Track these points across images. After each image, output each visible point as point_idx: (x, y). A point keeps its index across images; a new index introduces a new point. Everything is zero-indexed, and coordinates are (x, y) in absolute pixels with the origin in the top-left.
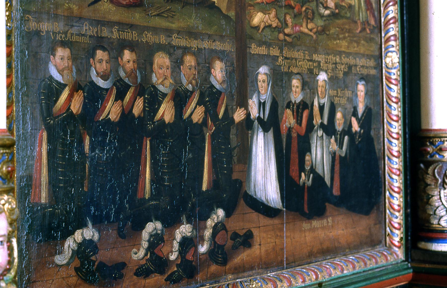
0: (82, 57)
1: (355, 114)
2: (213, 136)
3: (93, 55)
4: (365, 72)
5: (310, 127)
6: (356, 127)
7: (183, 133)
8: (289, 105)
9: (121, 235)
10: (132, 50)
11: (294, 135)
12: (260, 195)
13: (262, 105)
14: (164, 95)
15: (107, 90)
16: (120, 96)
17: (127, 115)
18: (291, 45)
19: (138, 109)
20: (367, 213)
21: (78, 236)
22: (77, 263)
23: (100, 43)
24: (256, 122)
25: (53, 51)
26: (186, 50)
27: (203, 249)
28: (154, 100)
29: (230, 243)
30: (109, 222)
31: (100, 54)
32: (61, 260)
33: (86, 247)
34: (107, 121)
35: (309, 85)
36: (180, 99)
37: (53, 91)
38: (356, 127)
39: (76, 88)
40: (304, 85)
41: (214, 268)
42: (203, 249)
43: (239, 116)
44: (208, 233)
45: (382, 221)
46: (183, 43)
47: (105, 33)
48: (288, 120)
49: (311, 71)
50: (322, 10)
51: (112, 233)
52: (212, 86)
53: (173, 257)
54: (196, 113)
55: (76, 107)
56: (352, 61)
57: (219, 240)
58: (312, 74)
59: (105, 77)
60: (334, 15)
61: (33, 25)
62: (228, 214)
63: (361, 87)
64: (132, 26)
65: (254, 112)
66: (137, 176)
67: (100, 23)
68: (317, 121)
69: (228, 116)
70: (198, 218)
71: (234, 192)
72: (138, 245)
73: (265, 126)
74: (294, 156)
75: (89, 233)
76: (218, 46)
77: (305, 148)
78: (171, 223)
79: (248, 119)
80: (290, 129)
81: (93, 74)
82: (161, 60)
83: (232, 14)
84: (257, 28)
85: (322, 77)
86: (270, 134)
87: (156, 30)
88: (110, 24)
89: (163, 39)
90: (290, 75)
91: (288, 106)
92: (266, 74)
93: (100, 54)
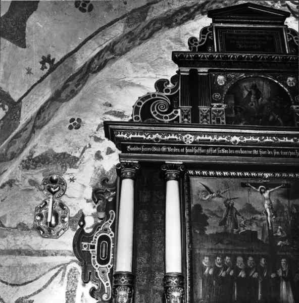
3: (216, 258)
10: (228, 256)
13: (284, 272)
14: (241, 269)
15: (220, 268)
17: (228, 275)
19: (231, 273)
23: (218, 255)
24: (281, 278)
26: (249, 256)
28: (237, 271)
31: (218, 258)
34: (221, 277)
36: (247, 270)
43: (273, 276)
52: (261, 266)
55: (211, 272)
59: (219, 264)
65: (280, 274)
73: (286, 279)
79: (277, 278)
81: (204, 199)
82: (240, 259)
87: (237, 250)
88: (221, 250)
89: (240, 253)
92: (284, 261)
93: (218, 258)
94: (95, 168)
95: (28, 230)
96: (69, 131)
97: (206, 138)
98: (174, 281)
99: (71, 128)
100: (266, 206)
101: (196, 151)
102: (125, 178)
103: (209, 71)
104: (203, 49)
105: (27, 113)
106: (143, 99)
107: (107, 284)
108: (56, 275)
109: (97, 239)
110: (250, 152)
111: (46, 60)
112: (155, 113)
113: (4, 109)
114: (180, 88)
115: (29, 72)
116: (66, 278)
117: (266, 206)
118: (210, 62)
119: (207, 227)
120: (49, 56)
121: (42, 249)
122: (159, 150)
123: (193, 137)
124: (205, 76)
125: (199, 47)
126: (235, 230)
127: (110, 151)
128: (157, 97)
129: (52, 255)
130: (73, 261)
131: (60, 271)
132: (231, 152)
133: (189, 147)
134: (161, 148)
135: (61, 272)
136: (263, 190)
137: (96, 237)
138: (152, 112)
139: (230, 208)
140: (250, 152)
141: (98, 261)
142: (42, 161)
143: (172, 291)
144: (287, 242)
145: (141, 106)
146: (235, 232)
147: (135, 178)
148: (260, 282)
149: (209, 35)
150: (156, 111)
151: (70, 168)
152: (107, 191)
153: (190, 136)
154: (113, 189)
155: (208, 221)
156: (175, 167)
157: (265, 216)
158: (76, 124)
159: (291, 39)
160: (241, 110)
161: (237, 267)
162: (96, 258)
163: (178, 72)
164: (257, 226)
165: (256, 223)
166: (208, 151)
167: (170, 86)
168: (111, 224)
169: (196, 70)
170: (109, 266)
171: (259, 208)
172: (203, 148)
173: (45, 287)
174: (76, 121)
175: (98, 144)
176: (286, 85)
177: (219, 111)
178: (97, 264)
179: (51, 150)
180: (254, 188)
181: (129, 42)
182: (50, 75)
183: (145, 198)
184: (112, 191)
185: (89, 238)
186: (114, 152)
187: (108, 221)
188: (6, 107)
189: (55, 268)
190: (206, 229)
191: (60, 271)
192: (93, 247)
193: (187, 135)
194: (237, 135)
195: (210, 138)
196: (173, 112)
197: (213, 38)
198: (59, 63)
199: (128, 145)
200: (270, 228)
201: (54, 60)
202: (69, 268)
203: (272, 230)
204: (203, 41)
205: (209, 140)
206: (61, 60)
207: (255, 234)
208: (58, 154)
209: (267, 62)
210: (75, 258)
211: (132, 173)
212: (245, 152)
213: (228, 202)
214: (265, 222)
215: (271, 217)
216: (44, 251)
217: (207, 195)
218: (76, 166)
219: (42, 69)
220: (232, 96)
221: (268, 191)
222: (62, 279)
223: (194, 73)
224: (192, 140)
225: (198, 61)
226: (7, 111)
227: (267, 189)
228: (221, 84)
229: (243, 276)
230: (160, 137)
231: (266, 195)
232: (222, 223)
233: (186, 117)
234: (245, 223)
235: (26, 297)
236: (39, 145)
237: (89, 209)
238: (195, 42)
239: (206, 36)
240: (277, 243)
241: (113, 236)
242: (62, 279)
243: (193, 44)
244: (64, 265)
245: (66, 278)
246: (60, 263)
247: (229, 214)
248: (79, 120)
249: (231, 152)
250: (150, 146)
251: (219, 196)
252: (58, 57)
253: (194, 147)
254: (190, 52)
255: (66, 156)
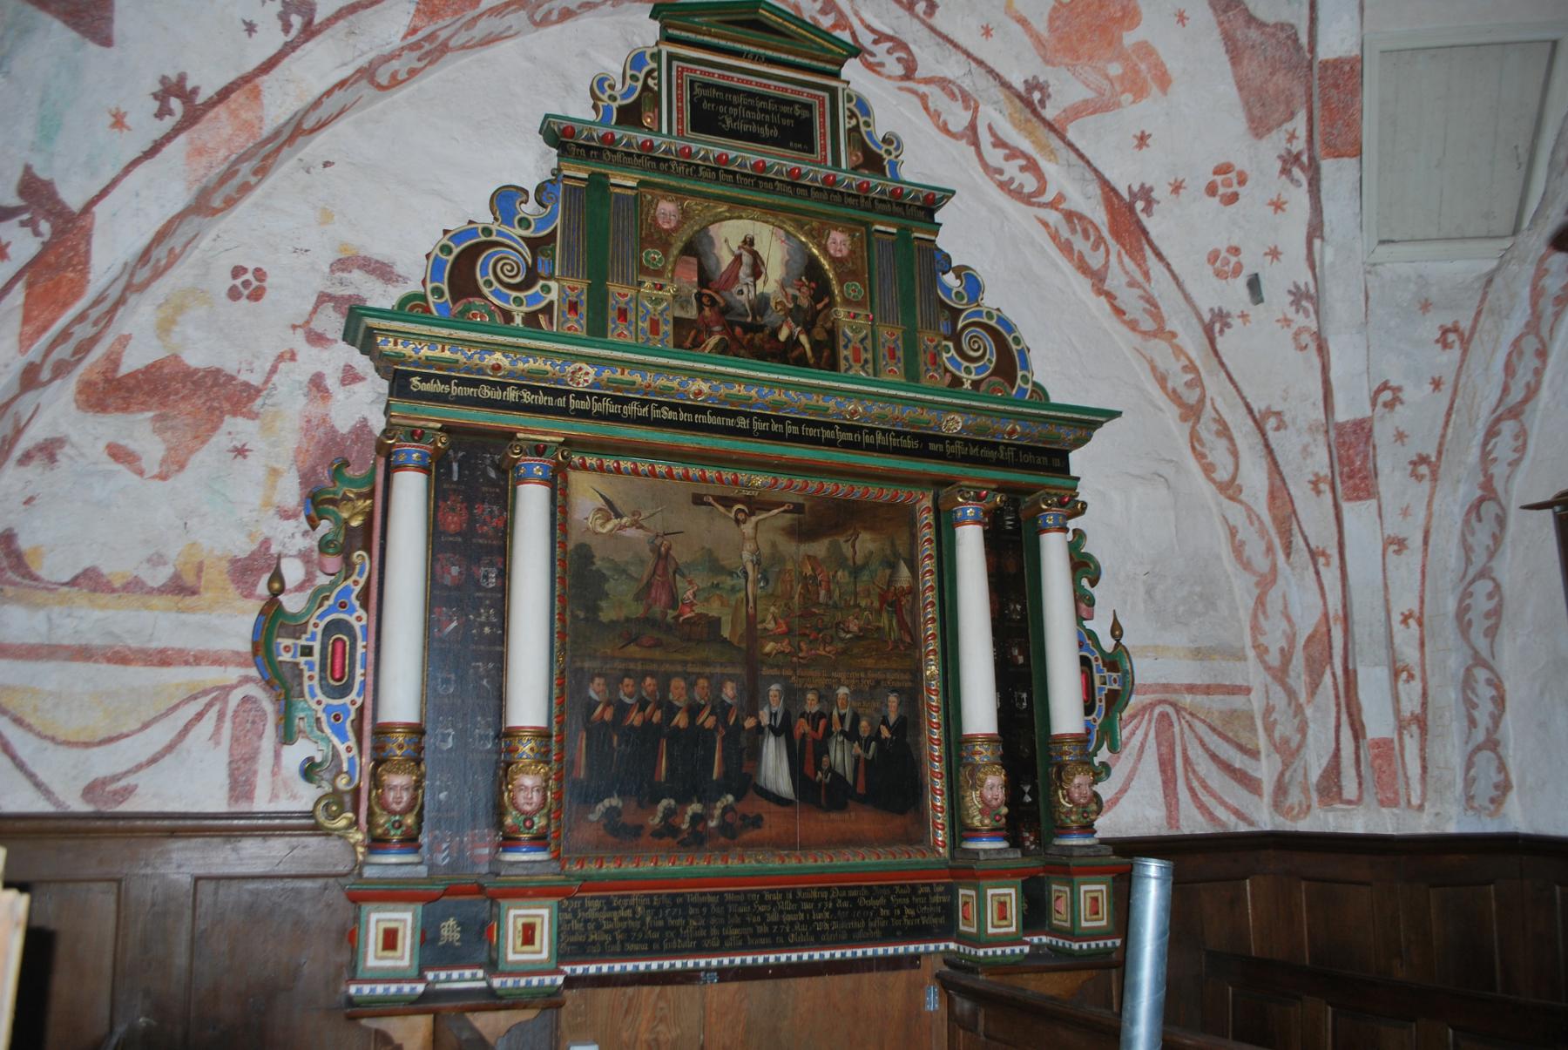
0: (614, 683)
1: (885, 721)
2: (723, 739)
4: (898, 685)
5: (828, 733)
6: (885, 733)
7: (696, 739)
8: (803, 715)
9: (640, 804)
11: (809, 739)
12: (771, 786)
13: (773, 715)
16: (642, 708)
17: (647, 722)
18: (806, 666)
19: (657, 717)
20: (902, 812)
21: (607, 802)
22: (605, 821)
23: (627, 673)
25: (592, 680)
27: (713, 824)
28: (671, 710)
29: (739, 823)
30: (531, 17)
31: (626, 680)
32: (593, 817)
33: (611, 811)
34: (632, 727)
35: (827, 696)
36: (694, 710)
37: (592, 705)
38: (885, 733)
39: (608, 704)
40: (820, 698)
41: (722, 840)
42: (713, 824)
43: (749, 723)
44: (717, 812)
45: (922, 819)
46: (697, 670)
47: (632, 666)
48: (802, 726)
49: (829, 687)
50: (843, 635)
51: (633, 804)
53: (685, 826)
54: (707, 720)
55: (608, 716)
56: (879, 675)
57: (728, 818)
58: (831, 689)
59: (630, 696)
60: (857, 638)
61: (578, 664)
62: (737, 799)
63: (893, 699)
64: (652, 661)
65: (765, 720)
66: (654, 767)
67: (626, 660)
68: (837, 727)
69: (739, 726)
70: (708, 799)
71: (744, 781)
72: (654, 814)
73: (776, 732)
74: (809, 757)
75: (615, 801)
76: (729, 670)
77: (822, 749)
78: (684, 800)
79: (759, 729)
80: (804, 735)
81: (600, 530)
82: (678, 684)
83: (743, 646)
84: (768, 655)
85: (843, 691)
86: (782, 739)
87: (672, 662)
88: (635, 660)
89: (679, 668)
90: (804, 691)
91: (803, 715)
93: (626, 680)
94: (309, 421)
95: (113, 591)
96: (229, 302)
97: (627, 377)
98: (526, 748)
99: (234, 294)
100: (746, 555)
101: (597, 407)
102: (402, 467)
103: (642, 183)
104: (630, 115)
105: (112, 247)
106: (458, 237)
107: (349, 749)
108: (200, 716)
109: (319, 631)
110: (730, 422)
111: (173, 89)
112: (489, 283)
113: (37, 233)
114: (558, 221)
115: (119, 121)
116: (227, 725)
117: (746, 555)
118: (648, 159)
119: (603, 604)
120: (182, 78)
121: (154, 645)
122: (497, 395)
123: (592, 371)
124: (628, 196)
125: (621, 109)
126: (671, 613)
127: (350, 377)
128: (494, 238)
129: (187, 663)
130: (246, 680)
131: (210, 705)
132: (683, 416)
133: (580, 396)
134: (503, 389)
135: (216, 708)
136: (741, 516)
137: (316, 625)
138: (481, 281)
139: (662, 557)
140: (730, 422)
141: (321, 687)
142: (146, 388)
143: (521, 771)
144: (784, 646)
145: (451, 258)
146: (669, 618)
147: (435, 469)
148: (719, 738)
149: (649, 74)
150: (492, 278)
151: (234, 414)
152: (345, 498)
153: (586, 368)
154: (365, 490)
155: (606, 586)
156: (539, 450)
157: (743, 581)
158: (249, 286)
159: (854, 122)
160: (713, 302)
161: (670, 704)
162: (316, 682)
163: (557, 172)
164: (723, 605)
165: (720, 597)
166: (629, 410)
167: (530, 208)
168: (357, 589)
169: (606, 176)
170: (353, 702)
171: (727, 560)
172: (616, 400)
173: (170, 748)
174: (249, 276)
175: (315, 351)
176: (824, 250)
177: (658, 301)
178: (320, 696)
179: (176, 357)
180: (721, 509)
181: (419, 60)
182: (182, 138)
183: (453, 522)
184: (360, 496)
185: (296, 627)
186: (363, 379)
187: (349, 582)
188: (45, 227)
189: (194, 697)
190: (601, 609)
191: (210, 705)
192: (307, 651)
193: (578, 365)
194: (706, 376)
195: (637, 378)
196: (537, 288)
197: (659, 84)
198: (212, 104)
199: (414, 374)
200: (751, 611)
201: (195, 91)
202: (235, 697)
203: (755, 616)
204: (631, 90)
205: (634, 383)
206: (218, 94)
207: (715, 623)
208: (196, 371)
209: (788, 183)
210: (253, 672)
211: (423, 456)
212: (718, 421)
213: (658, 542)
214: (742, 594)
215: (756, 582)
216: (162, 651)
217: (609, 520)
218: (250, 412)
219: (160, 115)
220: (694, 260)
221: (754, 519)
222: (218, 728)
223: (598, 183)
224: (590, 378)
225: (614, 152)
226: (47, 237)
227: (752, 514)
228: (666, 226)
229: (682, 725)
230: (505, 362)
231: (748, 528)
232: (643, 594)
233: (573, 307)
234: (695, 595)
235: (116, 778)
236: (140, 341)
237: (293, 539)
238: (609, 92)
239: (641, 76)
240: (763, 647)
241: (364, 622)
242: (218, 728)
243: (605, 97)
244: (223, 688)
245: (227, 725)
246: (209, 685)
247: (659, 572)
248: (260, 274)
249: (683, 416)
250: (475, 383)
251: (637, 525)
252: (207, 83)
253: (591, 395)
254: (593, 123)
255: (222, 380)
